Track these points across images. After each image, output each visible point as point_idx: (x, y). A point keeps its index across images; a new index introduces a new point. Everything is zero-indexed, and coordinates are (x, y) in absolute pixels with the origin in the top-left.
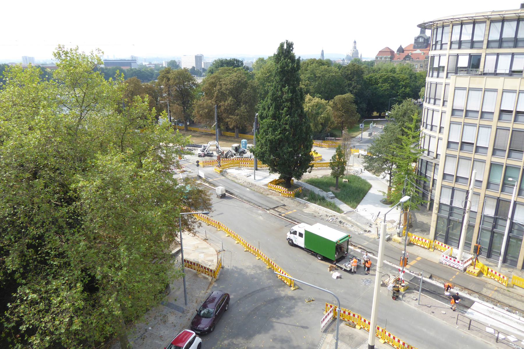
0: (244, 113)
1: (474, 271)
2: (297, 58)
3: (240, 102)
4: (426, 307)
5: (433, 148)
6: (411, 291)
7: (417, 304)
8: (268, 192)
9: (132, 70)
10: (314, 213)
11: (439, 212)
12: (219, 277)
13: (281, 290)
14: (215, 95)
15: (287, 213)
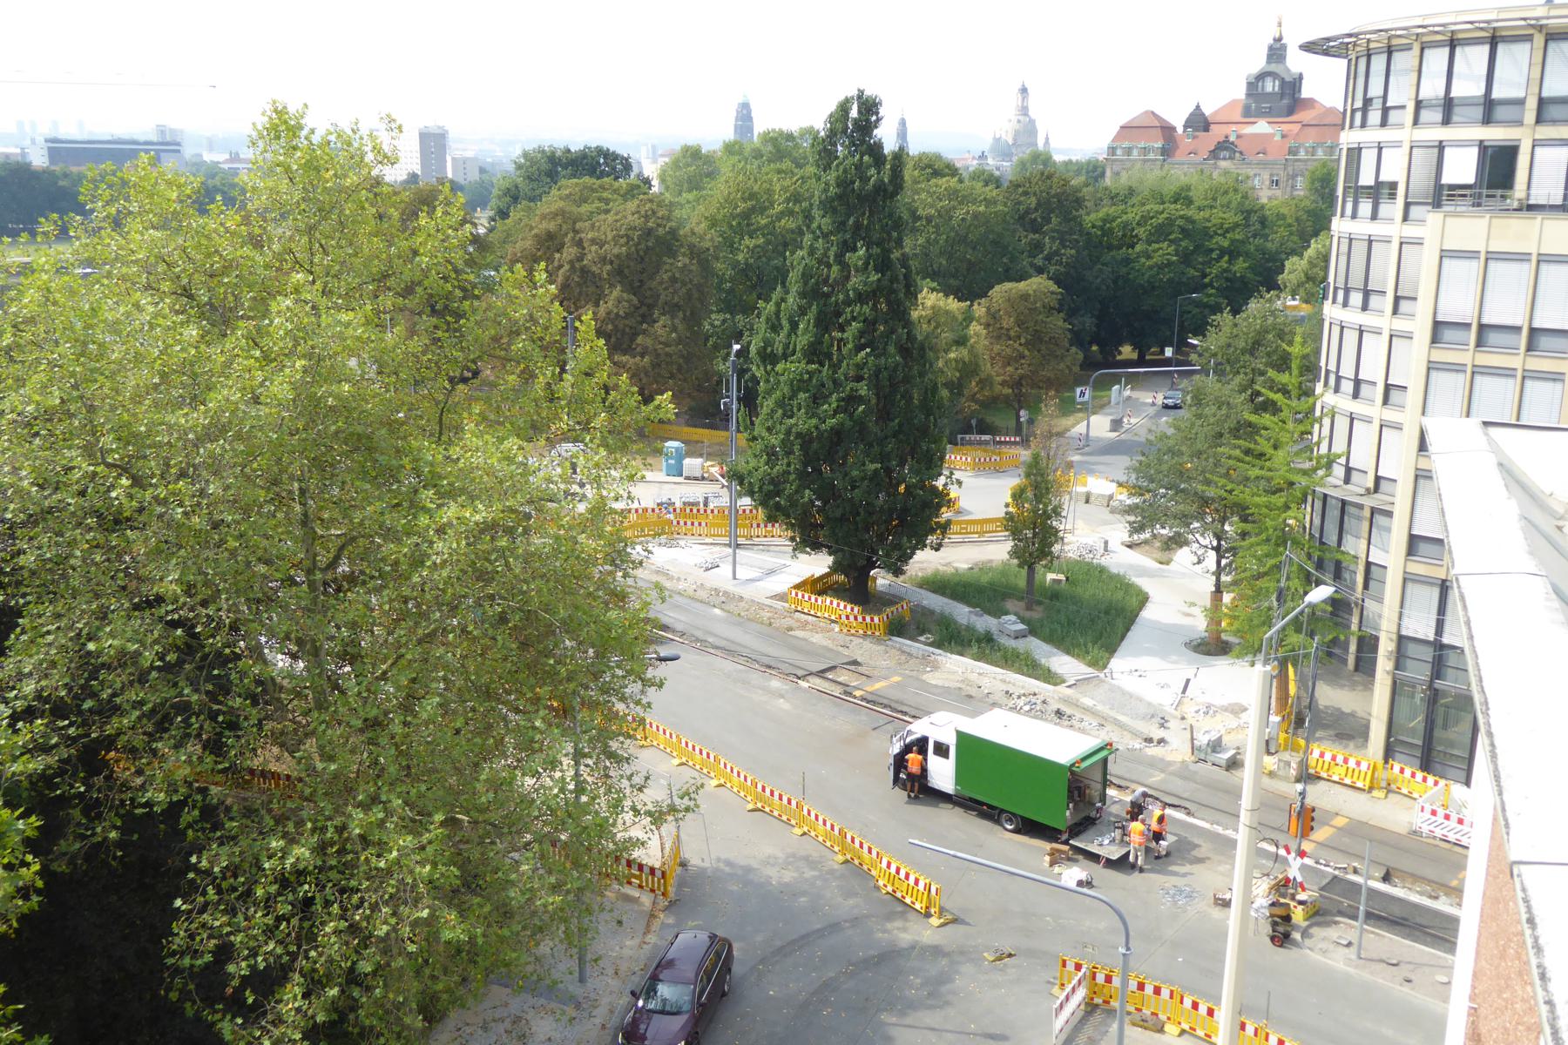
0: (667, 345)
3: (651, 307)
5: (1362, 457)
6: (1329, 918)
7: (1354, 957)
8: (788, 622)
11: (1397, 667)
13: (898, 929)
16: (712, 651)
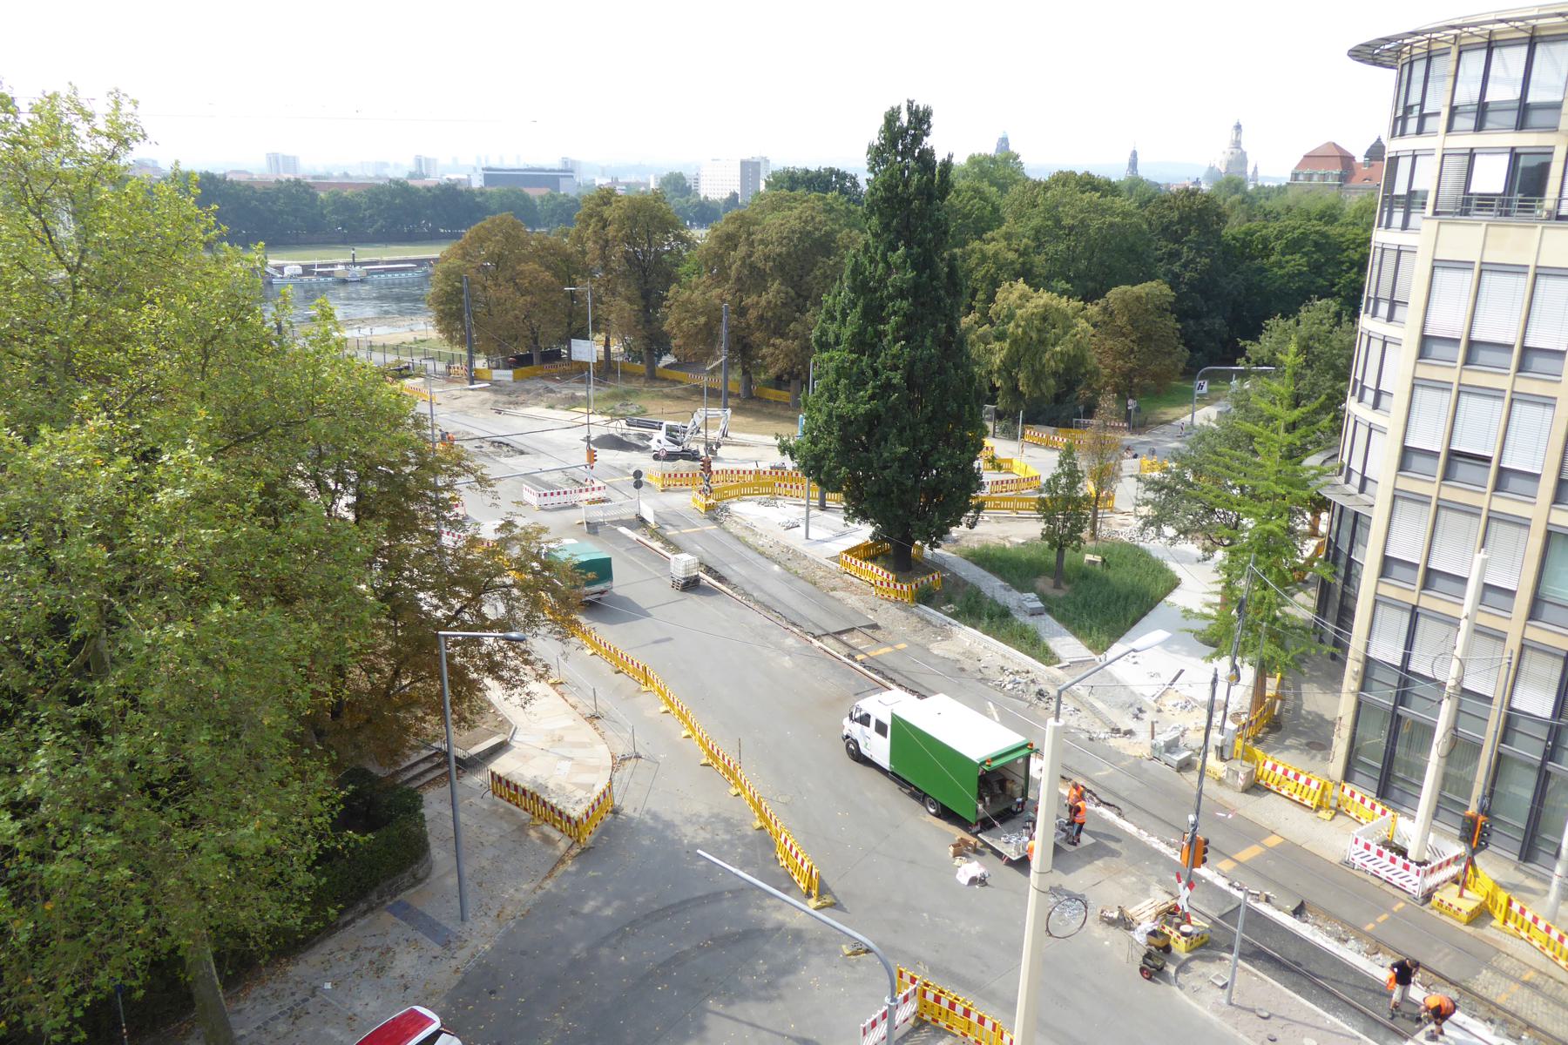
1: (1457, 903)
2: (939, 157)
4: (1254, 1017)
6: (1215, 953)
7: (1224, 1001)
8: (838, 582)
9: (553, 197)
10: (961, 658)
11: (1363, 688)
12: (595, 842)
14: (733, 273)
15: (872, 654)
16: (752, 605)
